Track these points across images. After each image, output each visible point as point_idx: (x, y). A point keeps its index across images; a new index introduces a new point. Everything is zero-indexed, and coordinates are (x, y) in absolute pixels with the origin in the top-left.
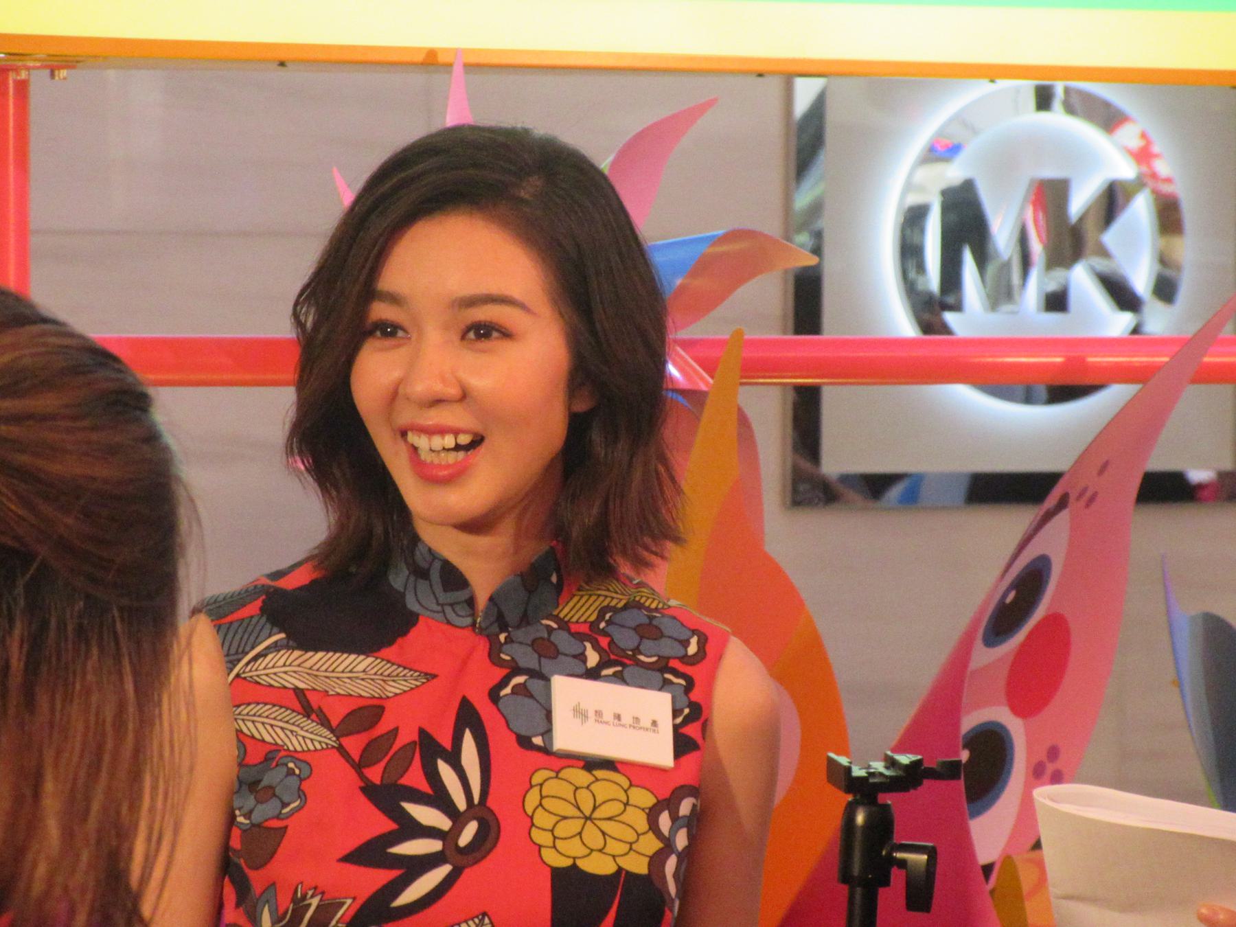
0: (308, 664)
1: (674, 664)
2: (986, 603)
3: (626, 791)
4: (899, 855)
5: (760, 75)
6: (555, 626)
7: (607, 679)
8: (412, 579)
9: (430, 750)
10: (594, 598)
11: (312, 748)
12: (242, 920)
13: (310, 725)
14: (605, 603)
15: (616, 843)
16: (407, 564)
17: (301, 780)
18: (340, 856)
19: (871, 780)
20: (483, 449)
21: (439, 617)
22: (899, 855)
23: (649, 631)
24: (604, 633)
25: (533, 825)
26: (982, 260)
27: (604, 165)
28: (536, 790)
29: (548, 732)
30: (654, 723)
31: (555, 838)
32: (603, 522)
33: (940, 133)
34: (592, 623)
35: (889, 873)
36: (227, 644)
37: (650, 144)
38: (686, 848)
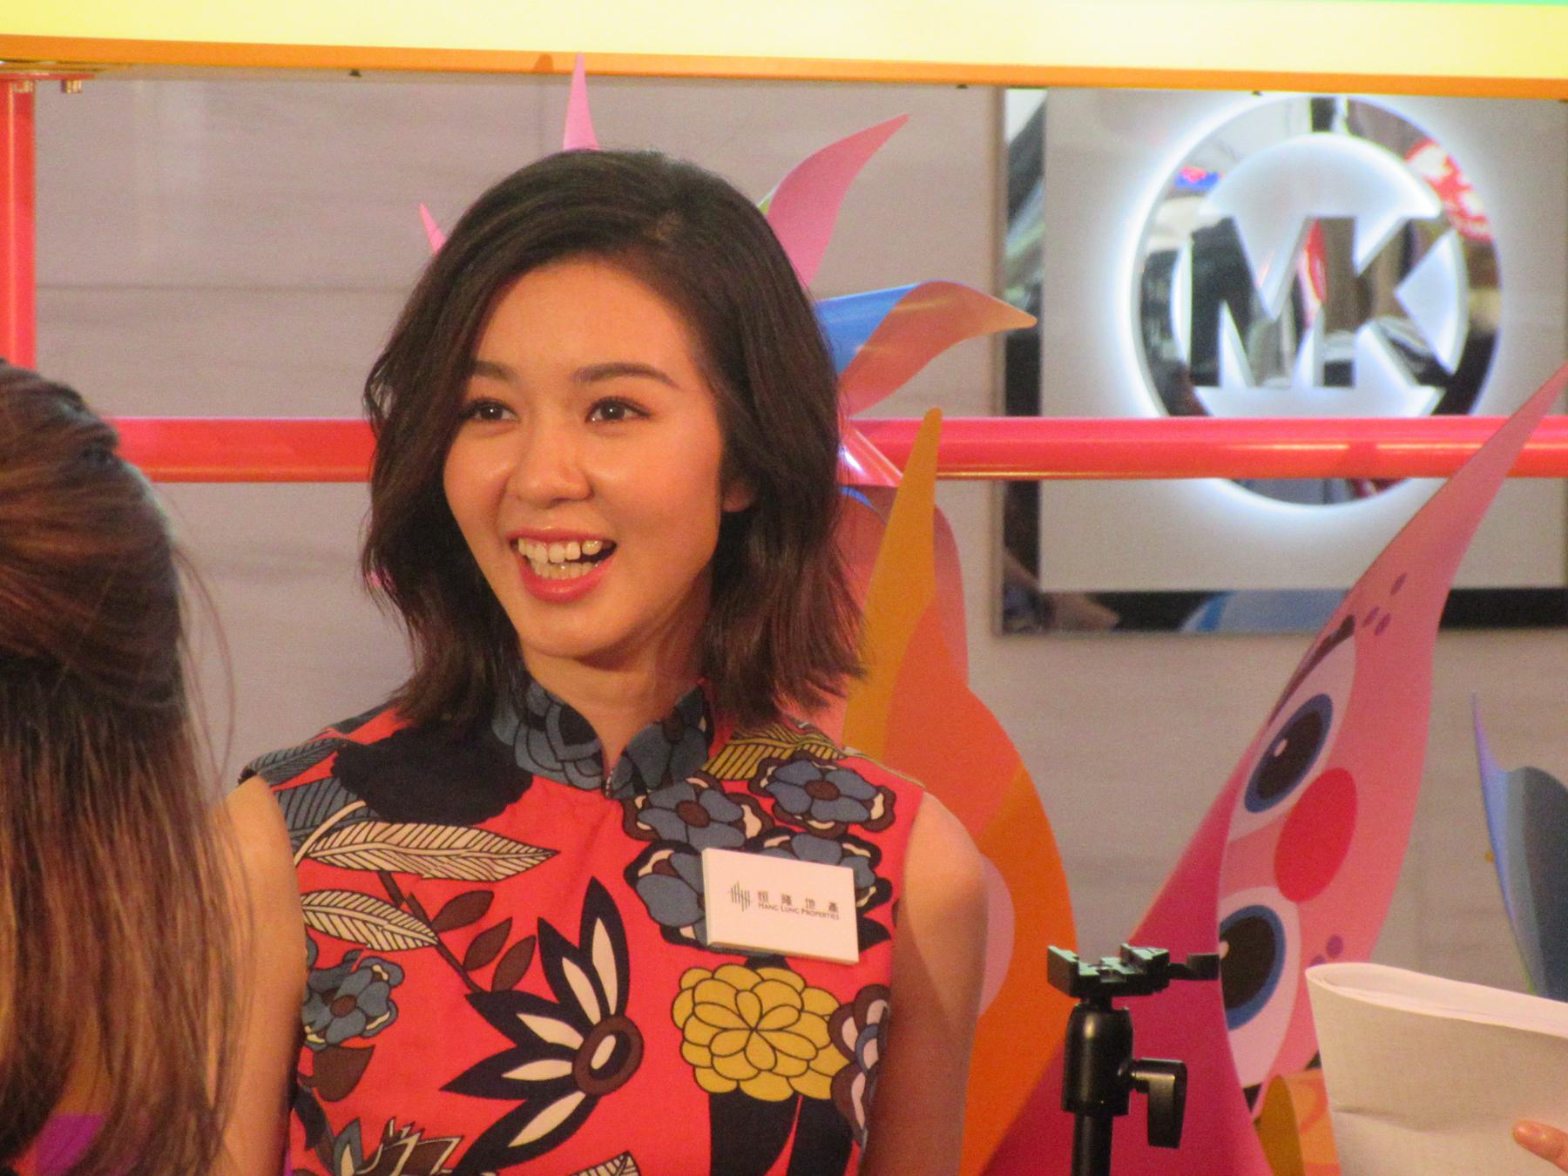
0: (396, 839)
1: (855, 830)
2: (1249, 755)
3: (800, 994)
4: (1139, 1075)
5: (962, 86)
6: (704, 785)
7: (771, 851)
8: (523, 731)
9: (553, 947)
10: (751, 748)
11: (403, 946)
12: (315, 1165)
13: (397, 916)
14: (766, 755)
15: (789, 1060)
16: (515, 705)
17: (391, 987)
18: (447, 1079)
19: (1104, 981)
20: (615, 559)
21: (560, 777)
22: (1139, 1075)
23: (823, 789)
24: (766, 793)
25: (684, 1039)
26: (1244, 320)
27: (763, 202)
28: (687, 995)
29: (700, 921)
30: (833, 907)
31: (713, 1055)
32: (765, 652)
33: (1191, 158)
34: (751, 780)
35: (1127, 1096)
36: (291, 816)
37: (818, 177)
38: (876, 1063)
